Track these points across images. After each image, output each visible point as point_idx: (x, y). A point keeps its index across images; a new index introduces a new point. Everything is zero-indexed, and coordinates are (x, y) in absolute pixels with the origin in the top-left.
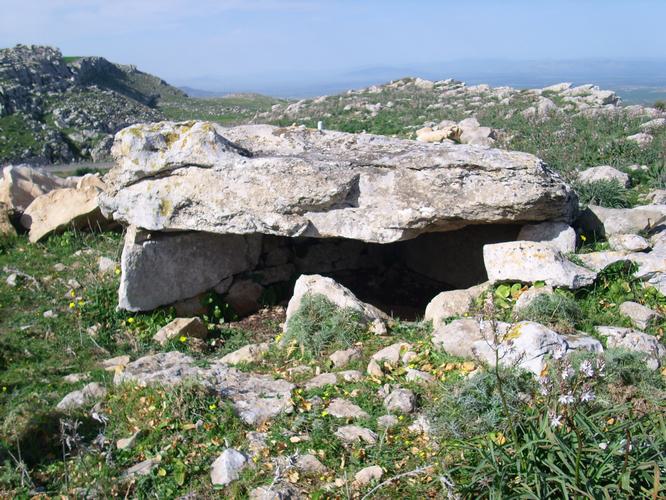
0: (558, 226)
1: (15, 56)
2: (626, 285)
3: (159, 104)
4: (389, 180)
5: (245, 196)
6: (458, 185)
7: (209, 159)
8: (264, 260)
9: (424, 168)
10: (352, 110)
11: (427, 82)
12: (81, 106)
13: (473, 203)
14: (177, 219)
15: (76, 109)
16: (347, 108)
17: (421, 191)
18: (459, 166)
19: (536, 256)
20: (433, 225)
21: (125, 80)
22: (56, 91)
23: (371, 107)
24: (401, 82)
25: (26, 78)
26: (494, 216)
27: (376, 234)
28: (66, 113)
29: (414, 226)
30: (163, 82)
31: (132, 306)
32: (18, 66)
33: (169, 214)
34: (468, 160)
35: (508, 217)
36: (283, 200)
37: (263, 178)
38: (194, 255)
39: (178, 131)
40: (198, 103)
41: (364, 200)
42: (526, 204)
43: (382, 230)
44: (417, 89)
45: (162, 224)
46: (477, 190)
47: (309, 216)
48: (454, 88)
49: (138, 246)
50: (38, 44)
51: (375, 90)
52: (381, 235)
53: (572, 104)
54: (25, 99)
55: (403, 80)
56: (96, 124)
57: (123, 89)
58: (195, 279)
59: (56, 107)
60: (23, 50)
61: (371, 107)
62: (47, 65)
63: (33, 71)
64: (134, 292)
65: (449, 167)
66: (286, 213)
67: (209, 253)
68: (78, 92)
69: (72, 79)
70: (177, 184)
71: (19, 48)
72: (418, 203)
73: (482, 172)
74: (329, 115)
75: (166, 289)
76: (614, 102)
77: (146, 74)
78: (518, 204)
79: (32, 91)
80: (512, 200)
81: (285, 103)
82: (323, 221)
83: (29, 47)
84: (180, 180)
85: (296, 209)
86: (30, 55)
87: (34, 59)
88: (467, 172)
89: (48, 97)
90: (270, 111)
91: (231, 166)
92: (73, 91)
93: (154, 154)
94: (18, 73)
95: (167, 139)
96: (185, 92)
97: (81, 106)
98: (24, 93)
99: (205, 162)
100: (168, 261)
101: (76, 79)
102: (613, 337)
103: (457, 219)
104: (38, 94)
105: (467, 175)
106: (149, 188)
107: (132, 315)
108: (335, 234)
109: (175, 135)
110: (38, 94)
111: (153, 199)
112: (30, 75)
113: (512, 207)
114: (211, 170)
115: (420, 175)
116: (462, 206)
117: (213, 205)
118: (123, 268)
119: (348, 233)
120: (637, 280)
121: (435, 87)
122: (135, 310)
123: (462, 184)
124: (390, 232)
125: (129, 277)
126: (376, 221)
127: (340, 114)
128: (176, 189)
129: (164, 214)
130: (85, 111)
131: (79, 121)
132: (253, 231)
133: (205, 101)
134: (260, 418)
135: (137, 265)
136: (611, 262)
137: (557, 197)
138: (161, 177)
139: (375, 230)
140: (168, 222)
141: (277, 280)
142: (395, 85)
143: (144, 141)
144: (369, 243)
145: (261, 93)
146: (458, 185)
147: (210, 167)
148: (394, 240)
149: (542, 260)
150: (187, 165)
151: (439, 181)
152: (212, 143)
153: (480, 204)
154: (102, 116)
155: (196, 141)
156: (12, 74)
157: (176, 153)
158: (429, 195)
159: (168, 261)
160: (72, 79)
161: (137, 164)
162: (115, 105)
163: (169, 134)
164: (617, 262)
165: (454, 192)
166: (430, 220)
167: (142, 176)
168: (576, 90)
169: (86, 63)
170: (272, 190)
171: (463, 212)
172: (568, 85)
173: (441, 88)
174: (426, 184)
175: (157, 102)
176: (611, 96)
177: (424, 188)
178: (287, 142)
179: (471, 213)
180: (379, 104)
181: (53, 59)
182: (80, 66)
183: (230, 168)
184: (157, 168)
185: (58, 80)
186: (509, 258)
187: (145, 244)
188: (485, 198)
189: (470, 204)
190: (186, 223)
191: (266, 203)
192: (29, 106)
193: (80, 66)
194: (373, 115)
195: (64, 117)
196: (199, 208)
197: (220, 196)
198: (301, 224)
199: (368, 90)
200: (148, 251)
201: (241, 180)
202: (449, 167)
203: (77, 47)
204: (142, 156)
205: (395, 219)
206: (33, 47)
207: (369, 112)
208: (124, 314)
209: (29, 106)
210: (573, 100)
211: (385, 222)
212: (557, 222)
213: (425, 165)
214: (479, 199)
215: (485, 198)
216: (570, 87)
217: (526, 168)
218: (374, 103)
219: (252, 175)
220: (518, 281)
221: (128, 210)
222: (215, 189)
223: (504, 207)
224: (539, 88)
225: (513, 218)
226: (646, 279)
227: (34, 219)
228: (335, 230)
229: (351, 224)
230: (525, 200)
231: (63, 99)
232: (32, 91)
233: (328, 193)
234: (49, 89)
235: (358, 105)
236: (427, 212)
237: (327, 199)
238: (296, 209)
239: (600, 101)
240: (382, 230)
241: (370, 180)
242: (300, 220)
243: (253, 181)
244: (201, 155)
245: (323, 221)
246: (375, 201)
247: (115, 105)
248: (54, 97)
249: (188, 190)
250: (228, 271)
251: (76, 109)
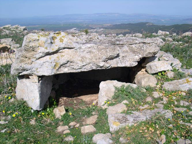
4: (126, 48)
5: (90, 57)
9: (134, 44)
13: (147, 52)
14: (60, 70)
17: (136, 50)
18: (141, 43)
33: (57, 68)
36: (104, 57)
41: (121, 55)
43: (132, 63)
48: (79, 30)
52: (132, 64)
53: (15, 31)
70: (62, 56)
72: (137, 54)
76: (26, 30)
84: (63, 54)
91: (81, 47)
99: (72, 47)
106: (50, 59)
108: (116, 66)
109: (55, 37)
111: (53, 63)
115: (133, 46)
117: (79, 62)
124: (134, 63)
132: (92, 69)
139: (131, 63)
140: (56, 71)
144: (129, 68)
145: (178, 24)
147: (72, 48)
148: (136, 65)
150: (64, 48)
151: (140, 47)
153: (149, 53)
161: (47, 49)
167: (48, 54)
168: (14, 27)
170: (100, 54)
172: (10, 25)
174: (136, 48)
176: (25, 28)
177: (136, 50)
183: (80, 48)
184: (54, 50)
186: (161, 65)
188: (150, 51)
191: (99, 59)
196: (72, 64)
197: (80, 59)
201: (85, 52)
210: (14, 29)
211: (133, 60)
213: (134, 43)
214: (148, 51)
216: (11, 26)
219: (89, 50)
221: (37, 69)
224: (1, 27)
228: (116, 65)
229: (121, 62)
233: (117, 53)
238: (107, 60)
239: (22, 30)
240: (132, 63)
243: (90, 52)
244: (71, 44)
246: (125, 55)
249: (68, 58)
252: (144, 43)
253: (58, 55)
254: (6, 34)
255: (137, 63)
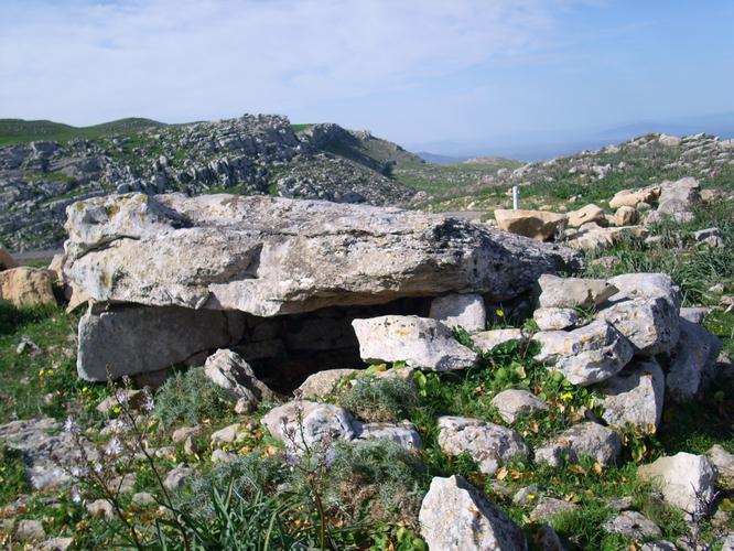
0: (463, 299)
1: (242, 126)
2: (520, 370)
3: (394, 172)
4: (284, 250)
6: (342, 253)
7: (136, 230)
8: (251, 335)
10: (578, 172)
11: (672, 138)
12: (307, 176)
15: (301, 178)
16: (572, 171)
17: (307, 260)
18: (347, 232)
19: (398, 332)
20: (315, 297)
21: (359, 147)
22: (281, 160)
23: (598, 169)
24: (642, 139)
25: (252, 148)
26: (375, 287)
27: (259, 306)
28: (291, 183)
29: (294, 299)
30: (399, 148)
31: (90, 376)
32: (243, 136)
33: (110, 285)
34: (357, 225)
35: (392, 289)
36: (185, 272)
37: (176, 249)
38: (158, 327)
39: (119, 204)
40: (436, 170)
42: (404, 273)
44: (658, 145)
45: (106, 295)
46: (361, 259)
47: (212, 288)
49: (95, 317)
50: (265, 113)
51: (612, 149)
54: (251, 168)
55: (646, 137)
56: (321, 193)
57: (357, 157)
58: (160, 352)
59: (281, 177)
60: (250, 120)
61: (598, 169)
62: (274, 134)
63: (258, 140)
64: (90, 362)
65: (339, 233)
66: (190, 285)
67: (176, 326)
68: (304, 161)
69: (299, 147)
71: (246, 118)
72: (300, 273)
73: (370, 238)
74: (550, 179)
75: (127, 361)
77: (380, 140)
78: (395, 274)
79: (257, 161)
80: (389, 269)
81: (510, 169)
82: (224, 293)
83: (257, 117)
85: (199, 280)
86: (256, 124)
87: (260, 129)
88: (352, 238)
89: (273, 167)
90: (496, 176)
91: (155, 236)
92: (299, 160)
93: (94, 226)
94: (243, 143)
95: (109, 212)
96: (423, 157)
97: (307, 176)
98: (249, 164)
100: (127, 332)
101: (302, 147)
102: (447, 428)
103: (338, 290)
104: (263, 164)
105: (353, 242)
107: (89, 384)
110: (263, 164)
112: (256, 145)
113: (390, 277)
114: (139, 242)
115: (311, 243)
116: (344, 276)
118: (79, 337)
119: (243, 306)
120: (539, 364)
121: (681, 144)
122: (93, 380)
123: (348, 252)
125: (83, 347)
126: (258, 297)
127: (564, 177)
128: (111, 260)
129: (106, 285)
130: (311, 181)
131: (304, 190)
132: (168, 303)
133: (443, 168)
134: (48, 484)
135: (92, 336)
136: (502, 341)
137: (444, 265)
138: (103, 250)
139: (259, 302)
141: (262, 355)
142: (636, 143)
143: (84, 214)
146: (342, 253)
147: (138, 238)
149: (405, 337)
150: (122, 237)
151: (324, 249)
152: (143, 215)
154: (327, 186)
155: (126, 213)
156: (238, 144)
157: (113, 226)
158: (313, 265)
159: (127, 332)
160: (299, 147)
162: (342, 173)
163: (111, 207)
164: (510, 341)
165: (338, 260)
166: (309, 291)
167: (88, 249)
169: (319, 130)
171: (345, 283)
173: (688, 144)
175: (392, 170)
178: (230, 212)
179: (354, 283)
180: (608, 165)
181: (280, 127)
182: (311, 134)
183: (153, 239)
185: (284, 149)
186: (373, 334)
187: (102, 315)
189: (352, 274)
190: (124, 295)
192: (253, 177)
193: (311, 134)
194: (600, 177)
195: (288, 187)
198: (198, 295)
199: (604, 149)
200: (105, 322)
202: (339, 233)
203: (306, 111)
204: (83, 228)
205: (275, 290)
206: (260, 115)
207: (595, 174)
208: (82, 384)
209: (253, 177)
212: (465, 294)
213: (317, 232)
214: (360, 269)
215: (365, 266)
217: (412, 233)
218: (603, 164)
220: (381, 362)
222: (140, 261)
223: (385, 277)
225: (397, 289)
226: (551, 363)
227: (75, 291)
230: (402, 269)
231: (288, 168)
232: (257, 161)
233: (221, 263)
234: (274, 159)
235: (585, 167)
236: (306, 283)
237: (222, 270)
241: (271, 249)
242: (199, 291)
245: (224, 293)
247: (342, 173)
248: (278, 167)
250: (199, 345)
251: (301, 178)
252: (363, 233)
253: (105, 253)
254: (563, 378)
255: (278, 307)
